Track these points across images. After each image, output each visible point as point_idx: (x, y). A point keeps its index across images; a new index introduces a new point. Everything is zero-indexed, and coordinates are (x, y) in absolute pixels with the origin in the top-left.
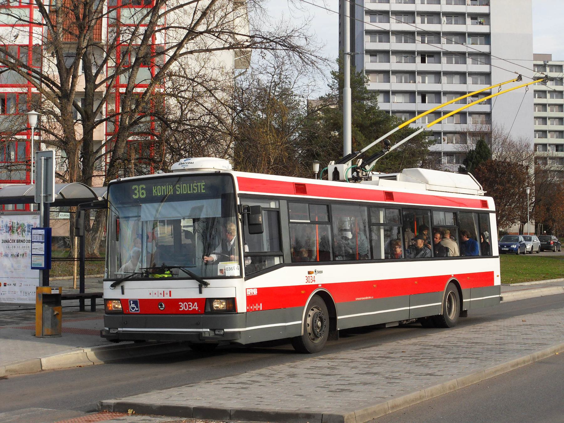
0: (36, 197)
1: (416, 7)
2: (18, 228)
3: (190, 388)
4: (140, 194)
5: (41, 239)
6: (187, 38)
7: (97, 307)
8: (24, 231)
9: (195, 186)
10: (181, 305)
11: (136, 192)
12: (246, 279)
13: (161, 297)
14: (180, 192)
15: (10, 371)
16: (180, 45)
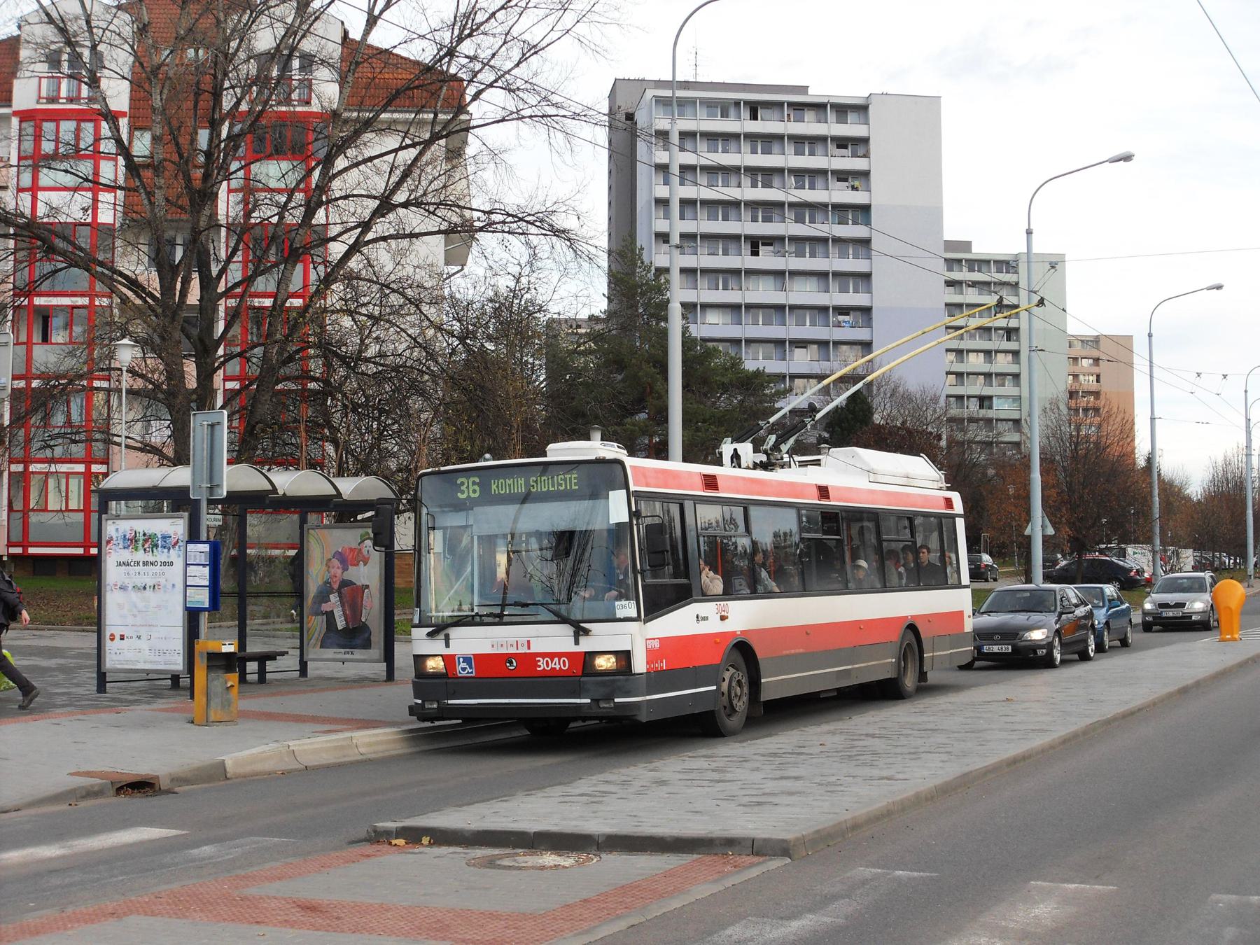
0: (193, 489)
1: (743, 158)
2: (146, 541)
3: (505, 804)
4: (471, 492)
5: (204, 559)
6: (379, 213)
7: (268, 676)
8: (156, 546)
9: (561, 479)
10: (539, 661)
11: (463, 488)
12: (645, 622)
13: (513, 651)
14: (566, 486)
15: (177, 780)
16: (366, 226)
